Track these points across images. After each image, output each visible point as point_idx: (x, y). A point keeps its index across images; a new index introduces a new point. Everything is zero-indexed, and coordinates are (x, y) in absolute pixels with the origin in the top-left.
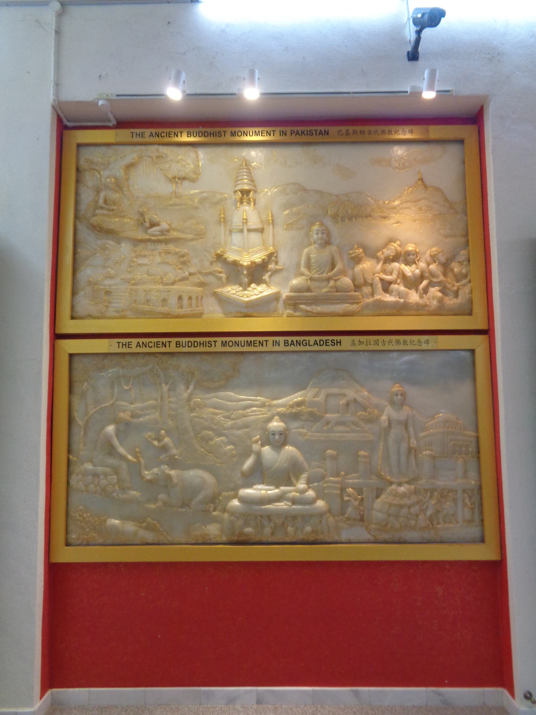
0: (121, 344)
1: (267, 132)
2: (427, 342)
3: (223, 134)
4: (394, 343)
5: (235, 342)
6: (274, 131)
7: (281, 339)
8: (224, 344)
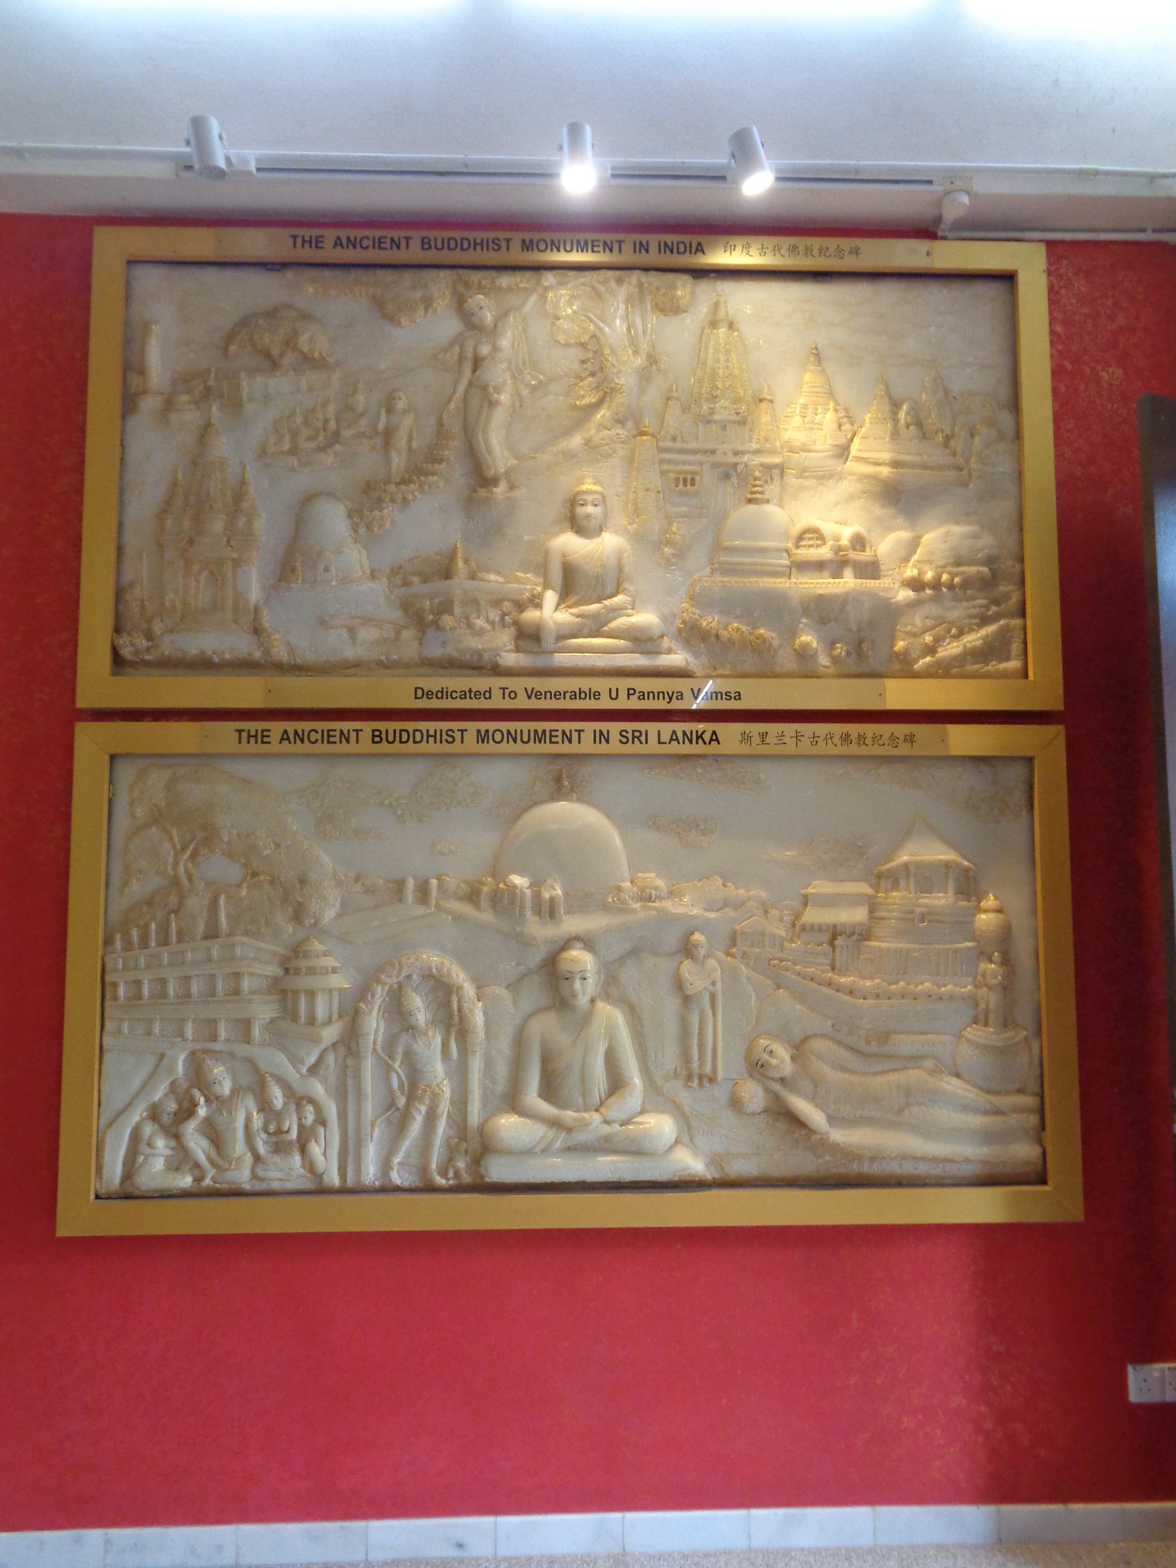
0: (245, 735)
2: (910, 739)
3: (504, 244)
4: (837, 740)
6: (620, 242)
7: (614, 728)
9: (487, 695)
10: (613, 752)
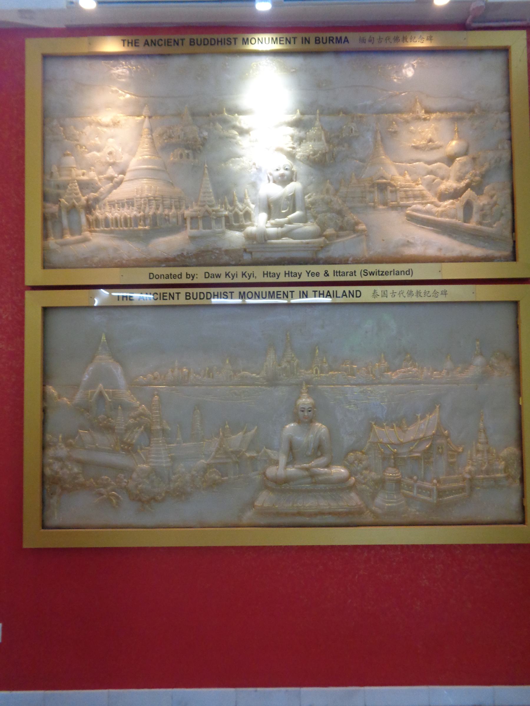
1: (287, 39)
2: (445, 293)
3: (233, 41)
4: (405, 294)
5: (256, 293)
6: (295, 38)
8: (188, 296)
9: (180, 276)
10: (181, 304)
